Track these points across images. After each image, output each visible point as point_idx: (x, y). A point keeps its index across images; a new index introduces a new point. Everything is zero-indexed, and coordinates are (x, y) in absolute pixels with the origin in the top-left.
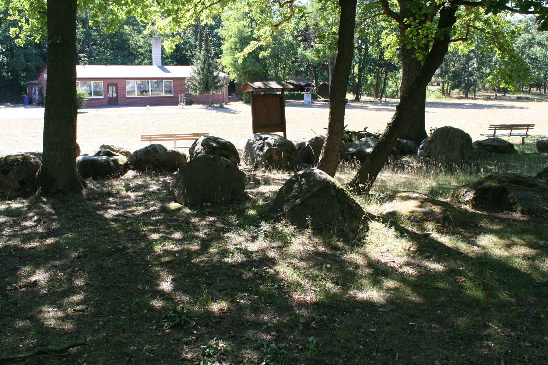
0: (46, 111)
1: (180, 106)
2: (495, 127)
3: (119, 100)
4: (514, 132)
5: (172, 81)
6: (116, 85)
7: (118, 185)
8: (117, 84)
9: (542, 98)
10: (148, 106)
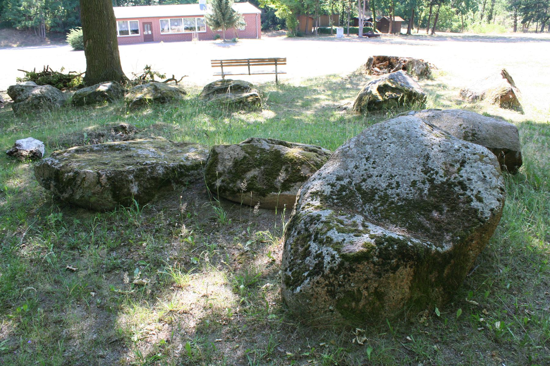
0: (87, 54)
1: (193, 42)
2: (70, 72)
4: (254, 69)
5: (138, 21)
6: (150, 23)
7: (278, 124)
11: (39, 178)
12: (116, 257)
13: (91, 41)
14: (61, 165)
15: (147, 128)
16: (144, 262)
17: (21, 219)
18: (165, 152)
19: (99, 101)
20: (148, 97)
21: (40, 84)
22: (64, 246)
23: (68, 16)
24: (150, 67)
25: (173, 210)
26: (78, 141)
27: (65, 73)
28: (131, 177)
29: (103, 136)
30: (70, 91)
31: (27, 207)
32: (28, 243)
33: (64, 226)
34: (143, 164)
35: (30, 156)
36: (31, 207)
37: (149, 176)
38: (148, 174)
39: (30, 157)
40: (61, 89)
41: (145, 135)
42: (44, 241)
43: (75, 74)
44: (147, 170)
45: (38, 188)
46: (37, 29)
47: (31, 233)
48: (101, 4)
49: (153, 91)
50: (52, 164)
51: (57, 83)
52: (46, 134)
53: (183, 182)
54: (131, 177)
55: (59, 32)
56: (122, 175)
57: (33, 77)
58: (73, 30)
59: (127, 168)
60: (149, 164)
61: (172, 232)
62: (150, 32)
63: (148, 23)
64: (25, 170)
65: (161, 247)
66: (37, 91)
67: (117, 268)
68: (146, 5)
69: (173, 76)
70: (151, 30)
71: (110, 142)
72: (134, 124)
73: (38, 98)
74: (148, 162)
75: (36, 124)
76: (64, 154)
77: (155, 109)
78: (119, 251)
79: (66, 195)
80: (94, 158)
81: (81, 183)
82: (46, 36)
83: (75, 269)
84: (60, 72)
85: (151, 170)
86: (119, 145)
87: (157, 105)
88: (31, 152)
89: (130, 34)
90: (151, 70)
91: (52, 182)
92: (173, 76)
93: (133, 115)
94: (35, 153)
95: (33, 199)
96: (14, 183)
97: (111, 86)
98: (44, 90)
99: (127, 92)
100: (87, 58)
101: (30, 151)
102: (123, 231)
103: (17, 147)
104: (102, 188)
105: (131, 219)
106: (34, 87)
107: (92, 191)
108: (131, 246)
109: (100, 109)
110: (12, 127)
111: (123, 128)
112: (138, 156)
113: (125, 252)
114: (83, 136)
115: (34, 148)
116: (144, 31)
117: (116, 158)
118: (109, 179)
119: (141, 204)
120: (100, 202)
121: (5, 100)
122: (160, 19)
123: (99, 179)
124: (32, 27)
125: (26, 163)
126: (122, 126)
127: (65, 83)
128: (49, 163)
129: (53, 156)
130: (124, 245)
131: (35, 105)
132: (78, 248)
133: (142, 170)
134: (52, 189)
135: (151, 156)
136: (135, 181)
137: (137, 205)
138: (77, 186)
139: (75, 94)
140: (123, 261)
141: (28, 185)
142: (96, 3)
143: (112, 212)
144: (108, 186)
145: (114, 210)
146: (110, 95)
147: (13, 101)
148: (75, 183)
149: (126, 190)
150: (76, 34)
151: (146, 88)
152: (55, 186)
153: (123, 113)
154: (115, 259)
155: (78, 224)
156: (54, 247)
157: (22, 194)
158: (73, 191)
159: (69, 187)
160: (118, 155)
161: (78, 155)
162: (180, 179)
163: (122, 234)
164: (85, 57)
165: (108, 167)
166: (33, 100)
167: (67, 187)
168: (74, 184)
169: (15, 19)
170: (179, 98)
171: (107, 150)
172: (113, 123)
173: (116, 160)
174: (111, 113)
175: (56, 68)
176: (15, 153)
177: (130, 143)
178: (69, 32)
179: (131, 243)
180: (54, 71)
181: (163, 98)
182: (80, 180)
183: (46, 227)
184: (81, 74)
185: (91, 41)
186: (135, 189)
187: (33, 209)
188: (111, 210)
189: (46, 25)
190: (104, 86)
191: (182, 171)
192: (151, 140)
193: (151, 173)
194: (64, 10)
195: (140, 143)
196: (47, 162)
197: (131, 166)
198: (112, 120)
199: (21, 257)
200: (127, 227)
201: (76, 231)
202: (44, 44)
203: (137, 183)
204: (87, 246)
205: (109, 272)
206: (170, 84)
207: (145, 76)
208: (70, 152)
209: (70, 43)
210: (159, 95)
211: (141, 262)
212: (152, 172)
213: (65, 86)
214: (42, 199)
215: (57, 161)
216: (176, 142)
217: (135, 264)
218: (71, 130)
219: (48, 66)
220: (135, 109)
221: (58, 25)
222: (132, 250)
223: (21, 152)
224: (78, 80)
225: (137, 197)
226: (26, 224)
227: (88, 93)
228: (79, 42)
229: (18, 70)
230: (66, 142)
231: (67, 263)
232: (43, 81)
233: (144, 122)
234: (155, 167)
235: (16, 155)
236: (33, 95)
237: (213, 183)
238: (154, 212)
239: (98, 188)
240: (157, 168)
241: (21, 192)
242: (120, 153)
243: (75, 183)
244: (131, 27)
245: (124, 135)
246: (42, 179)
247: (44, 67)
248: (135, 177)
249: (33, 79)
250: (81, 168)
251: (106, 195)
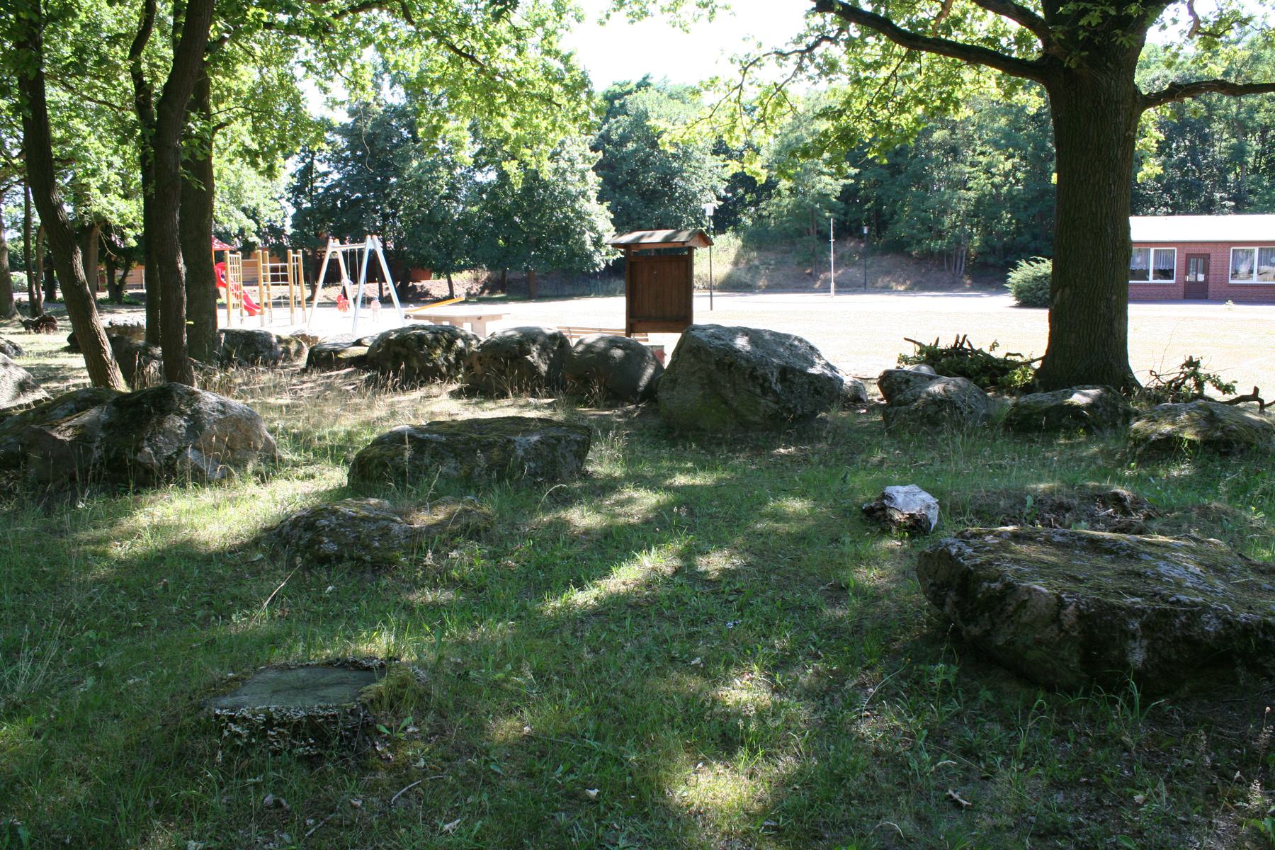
0: (1053, 320)
2: (1008, 354)
3: (1211, 289)
6: (1206, 257)
8: (1209, 255)
9: (1273, 212)
10: (1230, 304)
11: (925, 579)
12: (1062, 806)
13: (1067, 291)
14: (978, 561)
15: (1179, 509)
16: (1130, 842)
17: (870, 657)
18: (1227, 581)
19: (1067, 428)
20: (1189, 435)
21: (942, 372)
22: (950, 743)
23: (1018, 231)
24: (1198, 362)
25: (1226, 731)
26: (1010, 511)
27: (999, 354)
28: (1135, 625)
29: (1068, 509)
30: (1002, 394)
31: (886, 633)
32: (876, 712)
33: (957, 698)
34: (1171, 599)
35: (908, 524)
36: (894, 636)
37: (1178, 633)
38: (1179, 628)
39: (906, 527)
40: (984, 387)
41: (1174, 528)
42: (910, 717)
43: (1019, 359)
44: (1177, 616)
45: (915, 597)
46: (949, 256)
47: (889, 694)
48: (1104, 211)
49: (1203, 422)
50: (958, 555)
51: (977, 374)
52: (945, 482)
53: (1266, 668)
54: (1135, 625)
55: (993, 266)
56: (1115, 615)
57: (932, 355)
58: (1024, 263)
59: (1130, 600)
60: (1185, 605)
61: (1217, 789)
62: (1201, 278)
63: (1199, 254)
64: (892, 551)
65: (1183, 818)
66: (936, 388)
67: (1063, 834)
68: (1201, 214)
69: (1256, 390)
70: (1206, 271)
71: (1084, 530)
72: (1146, 495)
73: (939, 403)
74: (1182, 598)
75: (925, 458)
76: (988, 538)
77: (1203, 466)
78: (1073, 795)
79: (975, 630)
80: (1053, 559)
81: (1015, 611)
82: (966, 272)
83: (965, 803)
84: (986, 350)
85: (1188, 618)
86: (1115, 542)
87: (1208, 458)
88: (912, 516)
89: (1151, 280)
90: (1200, 371)
91: (952, 594)
92: (1256, 390)
93: (1144, 472)
94: (919, 520)
95: (901, 620)
96: (868, 576)
97: (1100, 397)
98: (951, 388)
99: (1138, 416)
100: (1051, 327)
101: (910, 515)
102: (1090, 750)
103: (885, 501)
104: (1062, 635)
105: (1112, 726)
106: (931, 378)
107: (1037, 636)
108: (1104, 792)
109: (1066, 445)
110: (878, 456)
111: (1118, 500)
112: (1159, 577)
113: (1087, 801)
114: (1024, 502)
115: (918, 508)
116: (1187, 273)
117: (1106, 570)
118: (1081, 616)
119: (1147, 697)
120: (1049, 665)
121: (869, 398)
122: (1232, 248)
123: (1058, 613)
124: (941, 253)
125: (896, 539)
126: (1116, 494)
127: (994, 376)
128: (954, 551)
129: (962, 536)
130: (1087, 783)
131: (929, 415)
132: (978, 756)
133: (1164, 614)
134: (947, 609)
135: (1190, 585)
136: (1142, 637)
137: (1137, 695)
138: (1004, 616)
139: (1015, 405)
140: (1081, 823)
141: (894, 586)
142: (1094, 210)
143: (1072, 696)
144: (1075, 634)
145: (1077, 691)
146: (1095, 417)
147: (884, 402)
148: (1002, 609)
149: (1116, 653)
150: (1024, 272)
151: (1187, 413)
152: (956, 604)
153: (1121, 463)
154: (1061, 810)
155: (988, 701)
156: (927, 738)
157: (880, 603)
158: (994, 624)
159: (987, 614)
160: (1109, 566)
161: (1018, 547)
162: (1260, 660)
163: (1087, 754)
164: (1047, 324)
165: (1082, 590)
166: (926, 404)
167: (982, 613)
168: (998, 609)
169: (913, 237)
170: (1271, 449)
171: (1083, 548)
172: (1097, 484)
173: (1104, 576)
174: (1093, 458)
175: (980, 342)
176: (879, 513)
177: (1141, 542)
178: (1015, 266)
179: (1106, 785)
180: (976, 348)
181: (1228, 444)
182: (1014, 603)
183: (918, 686)
184: (1033, 361)
185: (1067, 291)
186: (1137, 657)
187: (895, 640)
188: (1071, 690)
189: (968, 250)
190: (1085, 395)
191: (1269, 638)
192: (1193, 544)
193: (1185, 626)
194: (1010, 219)
195: (1164, 546)
196: (950, 548)
197: (1139, 600)
198: (1093, 477)
199: (858, 739)
200: (1102, 742)
201: (981, 715)
202: (957, 288)
203: (1145, 642)
204: (1000, 759)
205: (1040, 836)
206: (1244, 410)
207: (1183, 383)
208: (1000, 535)
209: (1013, 291)
210: (1219, 434)
211: (1124, 838)
212: (1189, 625)
213: (993, 383)
214: (918, 624)
215: (969, 550)
216: (1256, 561)
217: (1108, 841)
218: (1003, 484)
219: (965, 336)
220: (1150, 458)
221: (993, 250)
222: (1106, 802)
223: (892, 512)
224: (1025, 375)
225: (1140, 677)
226: (879, 669)
227: (1045, 406)
228: (1032, 289)
229: (906, 339)
230: (985, 508)
231: (950, 782)
232: (949, 368)
233: (1170, 496)
234: (1199, 614)
235: (879, 518)
236: (929, 394)
237: (84, 181)
238: (1174, 725)
239: (1051, 632)
240: (1205, 618)
241: (877, 598)
242: (1113, 562)
243: (1002, 609)
244: (1155, 263)
245: (1119, 516)
246: (931, 581)
247: (958, 337)
248: (1144, 626)
249: (932, 361)
250: (1021, 577)
251: (1065, 653)
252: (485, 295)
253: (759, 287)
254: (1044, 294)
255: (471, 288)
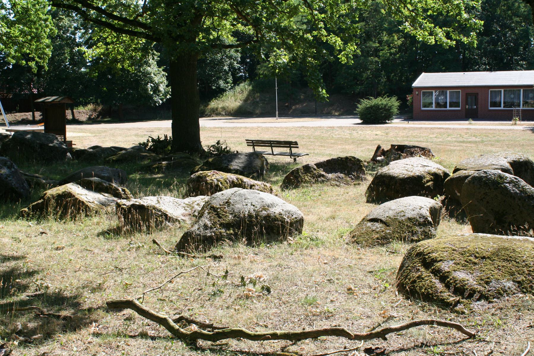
6: (476, 95)
8: (478, 94)
122: (490, 90)
252: (99, 119)
253: (256, 114)
254: (371, 116)
255: (92, 115)
